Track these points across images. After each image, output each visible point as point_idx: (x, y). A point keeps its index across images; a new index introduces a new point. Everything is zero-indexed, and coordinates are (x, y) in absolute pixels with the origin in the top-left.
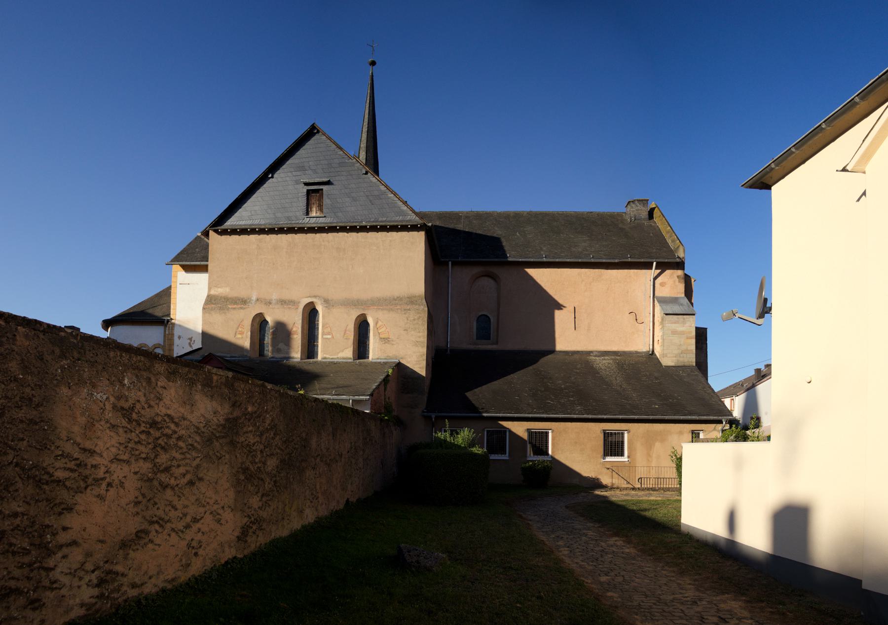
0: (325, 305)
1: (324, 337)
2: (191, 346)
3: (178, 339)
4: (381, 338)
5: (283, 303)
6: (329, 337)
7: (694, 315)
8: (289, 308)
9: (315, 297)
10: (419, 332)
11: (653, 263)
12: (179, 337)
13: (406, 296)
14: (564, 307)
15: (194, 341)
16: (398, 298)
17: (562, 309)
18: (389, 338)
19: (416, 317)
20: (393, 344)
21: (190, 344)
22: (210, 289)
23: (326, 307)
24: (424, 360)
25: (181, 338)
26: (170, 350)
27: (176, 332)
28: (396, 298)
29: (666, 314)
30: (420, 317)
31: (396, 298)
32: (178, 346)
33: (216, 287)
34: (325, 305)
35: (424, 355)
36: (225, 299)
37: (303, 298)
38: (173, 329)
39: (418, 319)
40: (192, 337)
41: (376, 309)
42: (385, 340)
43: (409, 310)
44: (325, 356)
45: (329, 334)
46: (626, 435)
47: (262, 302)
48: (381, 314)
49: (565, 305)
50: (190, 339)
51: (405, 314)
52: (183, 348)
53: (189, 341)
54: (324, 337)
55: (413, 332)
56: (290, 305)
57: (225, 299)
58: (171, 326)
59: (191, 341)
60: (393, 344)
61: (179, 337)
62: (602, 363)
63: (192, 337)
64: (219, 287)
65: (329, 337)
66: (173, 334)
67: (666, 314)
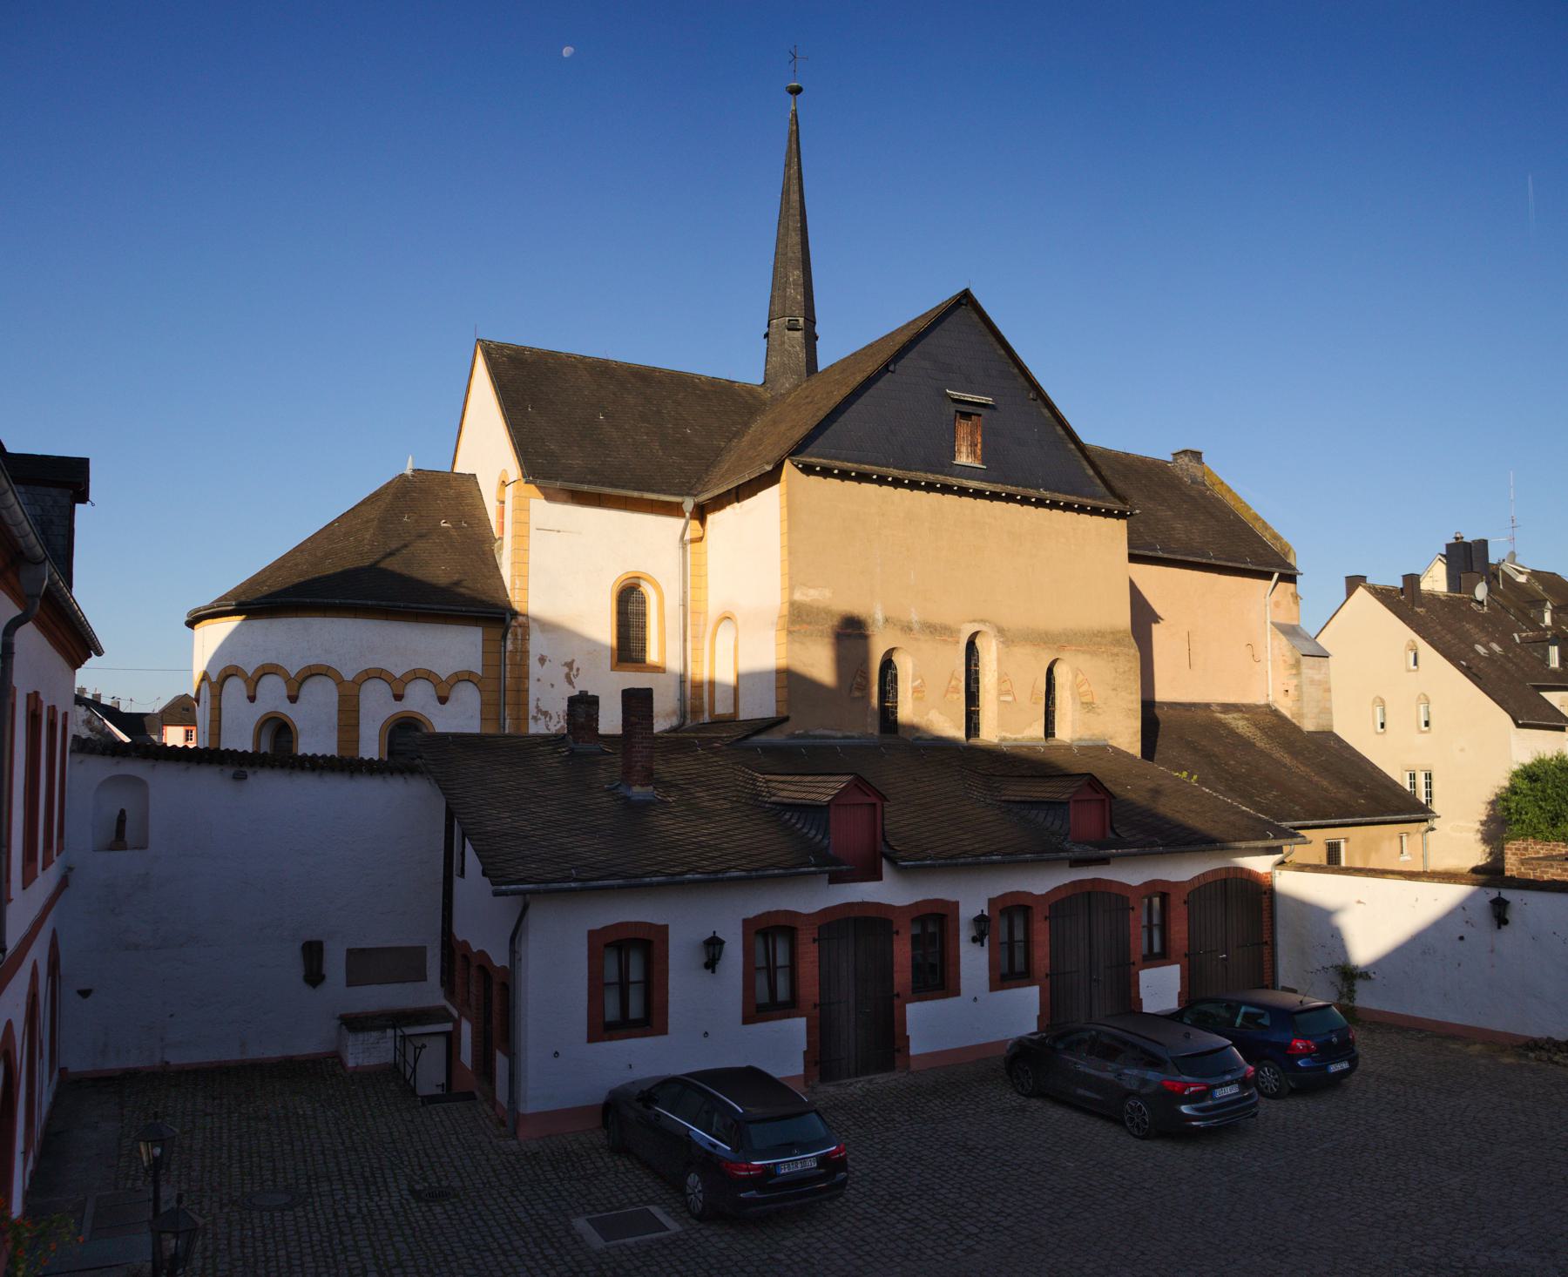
0: (1001, 640)
1: (1002, 698)
2: (570, 682)
3: (538, 663)
4: (1083, 703)
5: (932, 630)
6: (1009, 698)
7: (1327, 657)
8: (945, 641)
9: (983, 621)
10: (1131, 693)
11: (1273, 574)
12: (542, 660)
13: (1109, 630)
14: (1162, 619)
15: (578, 670)
16: (1099, 632)
17: (1159, 622)
18: (1093, 703)
19: (1127, 669)
20: (1099, 714)
21: (568, 677)
22: (792, 589)
23: (1003, 642)
24: (1137, 741)
25: (547, 663)
26: (518, 691)
27: (537, 644)
28: (1096, 632)
29: (1303, 655)
30: (1131, 668)
31: (1096, 632)
32: (539, 680)
33: (805, 585)
34: (1001, 640)
35: (1138, 732)
36: (826, 613)
37: (964, 622)
38: (525, 638)
39: (1130, 671)
40: (573, 661)
41: (1075, 650)
42: (1089, 706)
43: (1117, 655)
44: (1004, 734)
45: (1007, 693)
46: (1343, 845)
47: (895, 625)
48: (1084, 662)
49: (1162, 617)
50: (570, 665)
51: (1113, 661)
52: (552, 685)
53: (566, 670)
54: (1002, 698)
55: (1123, 694)
56: (944, 634)
57: (826, 613)
58: (519, 630)
59: (571, 669)
60: (1099, 714)
61: (542, 660)
62: (1239, 724)
63: (573, 661)
64: (810, 588)
65: (1009, 698)
66: (525, 653)
67: (1303, 655)
